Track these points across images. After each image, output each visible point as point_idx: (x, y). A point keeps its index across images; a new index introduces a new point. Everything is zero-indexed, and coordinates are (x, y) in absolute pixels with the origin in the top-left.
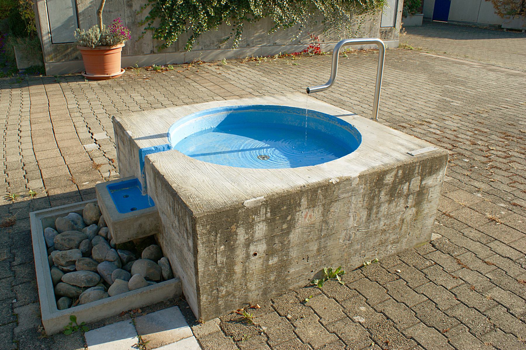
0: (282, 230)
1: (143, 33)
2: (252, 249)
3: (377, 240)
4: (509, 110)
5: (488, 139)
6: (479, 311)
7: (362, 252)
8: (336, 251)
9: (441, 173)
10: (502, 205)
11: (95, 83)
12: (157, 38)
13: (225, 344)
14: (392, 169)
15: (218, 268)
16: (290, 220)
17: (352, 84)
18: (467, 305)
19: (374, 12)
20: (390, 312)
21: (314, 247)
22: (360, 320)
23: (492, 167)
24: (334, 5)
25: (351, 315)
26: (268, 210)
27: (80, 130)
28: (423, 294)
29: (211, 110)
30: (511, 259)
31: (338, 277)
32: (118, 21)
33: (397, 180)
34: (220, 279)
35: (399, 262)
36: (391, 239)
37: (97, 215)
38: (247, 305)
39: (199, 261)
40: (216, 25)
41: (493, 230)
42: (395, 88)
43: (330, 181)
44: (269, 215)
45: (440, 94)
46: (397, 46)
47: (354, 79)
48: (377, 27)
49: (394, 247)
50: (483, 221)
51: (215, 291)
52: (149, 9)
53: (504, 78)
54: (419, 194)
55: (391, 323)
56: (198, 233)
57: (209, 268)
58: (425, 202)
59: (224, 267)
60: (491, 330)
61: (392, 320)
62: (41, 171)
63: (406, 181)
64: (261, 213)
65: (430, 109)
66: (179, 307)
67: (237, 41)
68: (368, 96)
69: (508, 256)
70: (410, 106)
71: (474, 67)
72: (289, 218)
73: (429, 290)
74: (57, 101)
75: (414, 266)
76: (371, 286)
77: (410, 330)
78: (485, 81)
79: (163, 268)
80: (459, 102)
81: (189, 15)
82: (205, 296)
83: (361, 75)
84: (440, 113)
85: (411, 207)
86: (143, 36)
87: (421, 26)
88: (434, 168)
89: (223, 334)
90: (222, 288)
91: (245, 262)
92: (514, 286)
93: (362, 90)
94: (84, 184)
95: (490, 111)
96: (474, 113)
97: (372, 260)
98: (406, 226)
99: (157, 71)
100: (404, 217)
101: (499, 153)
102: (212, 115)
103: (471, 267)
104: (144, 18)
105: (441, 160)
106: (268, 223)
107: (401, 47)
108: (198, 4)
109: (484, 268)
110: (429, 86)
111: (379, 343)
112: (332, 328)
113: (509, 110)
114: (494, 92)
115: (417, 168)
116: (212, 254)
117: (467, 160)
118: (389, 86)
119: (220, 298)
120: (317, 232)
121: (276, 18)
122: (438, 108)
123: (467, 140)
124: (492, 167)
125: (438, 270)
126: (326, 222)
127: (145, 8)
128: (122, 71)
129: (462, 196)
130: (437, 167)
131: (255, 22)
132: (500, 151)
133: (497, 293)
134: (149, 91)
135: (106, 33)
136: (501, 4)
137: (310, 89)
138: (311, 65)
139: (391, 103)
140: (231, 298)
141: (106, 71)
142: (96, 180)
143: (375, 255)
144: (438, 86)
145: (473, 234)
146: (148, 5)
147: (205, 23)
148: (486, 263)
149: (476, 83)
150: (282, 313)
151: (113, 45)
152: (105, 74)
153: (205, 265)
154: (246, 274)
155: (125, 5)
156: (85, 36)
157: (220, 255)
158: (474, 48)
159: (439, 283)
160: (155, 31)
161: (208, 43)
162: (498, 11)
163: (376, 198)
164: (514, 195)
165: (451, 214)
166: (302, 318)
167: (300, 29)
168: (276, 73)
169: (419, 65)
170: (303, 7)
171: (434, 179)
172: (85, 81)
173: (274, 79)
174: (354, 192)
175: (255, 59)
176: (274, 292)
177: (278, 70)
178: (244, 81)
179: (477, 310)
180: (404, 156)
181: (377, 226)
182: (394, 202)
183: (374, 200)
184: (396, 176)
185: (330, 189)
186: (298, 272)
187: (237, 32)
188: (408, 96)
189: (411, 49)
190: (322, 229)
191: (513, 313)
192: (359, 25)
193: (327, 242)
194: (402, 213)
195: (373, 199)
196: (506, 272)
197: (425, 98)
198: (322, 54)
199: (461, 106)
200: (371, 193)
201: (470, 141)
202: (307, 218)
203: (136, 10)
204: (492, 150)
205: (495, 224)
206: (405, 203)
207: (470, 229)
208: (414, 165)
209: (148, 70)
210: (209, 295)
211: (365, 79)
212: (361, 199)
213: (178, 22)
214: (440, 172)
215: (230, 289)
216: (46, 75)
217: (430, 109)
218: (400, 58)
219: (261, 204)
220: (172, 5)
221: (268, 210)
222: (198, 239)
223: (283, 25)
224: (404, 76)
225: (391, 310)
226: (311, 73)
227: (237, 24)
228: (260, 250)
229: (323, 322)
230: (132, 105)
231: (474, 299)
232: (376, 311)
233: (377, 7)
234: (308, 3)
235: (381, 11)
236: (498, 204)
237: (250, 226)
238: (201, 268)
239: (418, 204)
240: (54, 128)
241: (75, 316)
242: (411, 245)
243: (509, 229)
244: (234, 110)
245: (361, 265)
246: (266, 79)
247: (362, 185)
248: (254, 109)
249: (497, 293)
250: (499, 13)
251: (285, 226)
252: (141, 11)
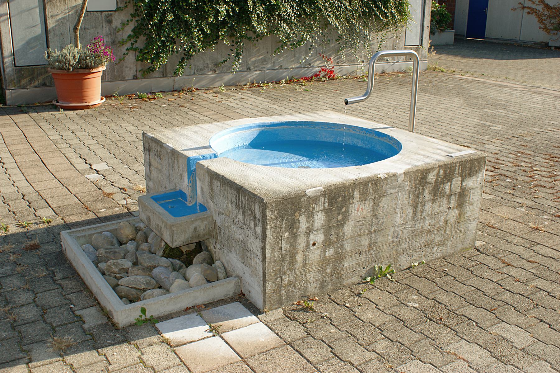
0: (338, 221)
1: (124, 54)
2: (312, 238)
3: (423, 240)
4: (556, 133)
5: (532, 160)
6: (523, 296)
7: (410, 251)
8: (385, 248)
9: (480, 175)
10: (546, 217)
11: (71, 113)
12: (142, 60)
13: (292, 326)
14: (434, 168)
15: (283, 255)
16: (345, 211)
17: (377, 110)
18: (512, 292)
19: (396, 27)
20: (441, 299)
21: (366, 242)
22: (414, 305)
23: (536, 186)
24: (349, 20)
25: (405, 302)
26: (326, 200)
27: (74, 161)
28: (470, 285)
29: (243, 126)
30: (553, 258)
31: (388, 276)
32: (99, 39)
33: (439, 179)
34: (283, 266)
35: (445, 263)
36: (436, 241)
37: (133, 232)
38: (306, 298)
39: (267, 246)
40: (212, 45)
41: (535, 237)
42: (427, 114)
43: (379, 176)
44: (327, 205)
45: (478, 118)
46: (425, 68)
47: (378, 104)
48: (401, 46)
49: (439, 249)
50: (527, 230)
51: (279, 279)
52: (132, 26)
53: (550, 101)
54: (460, 195)
55: (443, 306)
56: (268, 218)
57: (274, 255)
58: (467, 204)
59: (287, 255)
60: (534, 307)
61: (443, 304)
62: (45, 200)
63: (448, 181)
64: (320, 203)
65: (468, 134)
66: (241, 303)
67: (237, 63)
68: (396, 122)
69: (551, 256)
70: (445, 131)
71: (516, 90)
72: (344, 210)
73: (477, 283)
74: (33, 132)
75: (460, 266)
76: (421, 282)
77: (461, 310)
78: (529, 104)
79: (218, 270)
80: (501, 126)
81: (180, 33)
82: (270, 283)
83: (385, 101)
84: (479, 137)
85: (454, 208)
86: (124, 58)
87: (453, 45)
88: (473, 170)
89: (288, 319)
90: (284, 277)
91: (306, 252)
92: (554, 277)
93: (389, 116)
94: (101, 211)
95: (535, 134)
96: (516, 136)
97: (420, 261)
98: (450, 228)
99: (143, 100)
100: (447, 218)
101: (544, 173)
103: (515, 265)
104: (125, 37)
105: (479, 162)
106: (326, 213)
107: (431, 69)
108: (191, 19)
109: (527, 265)
110: (465, 110)
111: (434, 320)
112: (388, 312)
113: (556, 133)
114: (539, 115)
115: (457, 168)
116: (278, 240)
117: (510, 181)
118: (420, 111)
119: (283, 287)
120: (368, 226)
121: (283, 36)
122: (477, 132)
123: (510, 162)
124: (536, 186)
125: (483, 268)
126: (375, 216)
127: (128, 24)
128: (102, 99)
129: (504, 211)
130: (476, 169)
131: (257, 40)
132: (544, 171)
133: (539, 283)
134: (142, 121)
135: (85, 53)
136: (546, 18)
137: (349, 101)
138: (326, 91)
139: (424, 129)
140: (292, 288)
141: (84, 98)
142: (112, 208)
143: (421, 257)
144: (476, 110)
145: (517, 240)
146: (132, 20)
147: (199, 43)
148: (529, 261)
149: (519, 106)
150: (340, 303)
151: (92, 68)
152: (82, 103)
153: (272, 251)
154: (306, 264)
155: (104, 21)
156: (60, 57)
157: (284, 242)
158: (517, 69)
159: (485, 277)
160: (139, 52)
161: (201, 66)
162: (543, 25)
163: (420, 196)
164: (558, 209)
165: (494, 226)
166: (359, 305)
167: (310, 49)
168: (287, 100)
169: (453, 89)
170: (314, 23)
171: (474, 180)
172: (59, 111)
173: (285, 106)
174: (400, 189)
175: (257, 86)
176: (330, 287)
177: (288, 97)
178: (250, 109)
179: (521, 295)
180: (443, 158)
181: (423, 226)
182: (437, 201)
183: (419, 198)
184: (438, 174)
185: (379, 184)
186: (351, 267)
187: (237, 53)
188: (442, 121)
189: (442, 72)
190: (372, 223)
191: (554, 295)
192: (379, 43)
193: (377, 237)
194: (445, 214)
195: (418, 197)
196: (548, 268)
197: (461, 123)
198: (337, 79)
199: (502, 129)
200: (415, 191)
201: (513, 163)
202: (360, 211)
203: (116, 27)
204: (536, 170)
205: (539, 232)
206: (447, 204)
207: (513, 237)
208: (454, 165)
209: (132, 99)
210: (273, 283)
211: (392, 105)
212: (407, 196)
213: (168, 42)
214: (479, 174)
215: (291, 278)
216: (6, 105)
217: (468, 134)
218: (430, 82)
219: (320, 193)
220: (161, 21)
221: (326, 200)
222: (267, 224)
223: (291, 45)
224: (436, 101)
225: (441, 297)
226: (327, 99)
227: (237, 43)
228: (319, 240)
229: (380, 308)
230: (126, 135)
231: (518, 287)
232: (428, 298)
233: (400, 21)
234: (319, 18)
235: (405, 27)
236: (542, 217)
237: (311, 215)
238: (268, 254)
239: (460, 205)
240: (43, 160)
241: (144, 308)
242: (456, 249)
243: (551, 236)
244: (267, 126)
245: (409, 266)
246: (275, 107)
247: (407, 181)
248: (287, 125)
249: (539, 283)
250: (545, 28)
251: (340, 218)
252: (123, 29)
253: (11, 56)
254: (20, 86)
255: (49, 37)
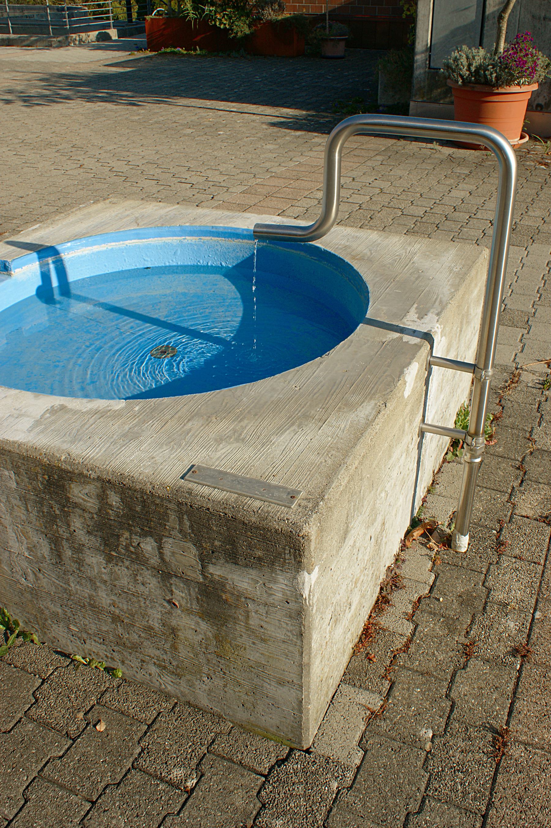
102: (221, 240)
128: (522, 137)
151: (497, 86)
253: (426, 50)
254: (431, 98)
255: (485, 28)
